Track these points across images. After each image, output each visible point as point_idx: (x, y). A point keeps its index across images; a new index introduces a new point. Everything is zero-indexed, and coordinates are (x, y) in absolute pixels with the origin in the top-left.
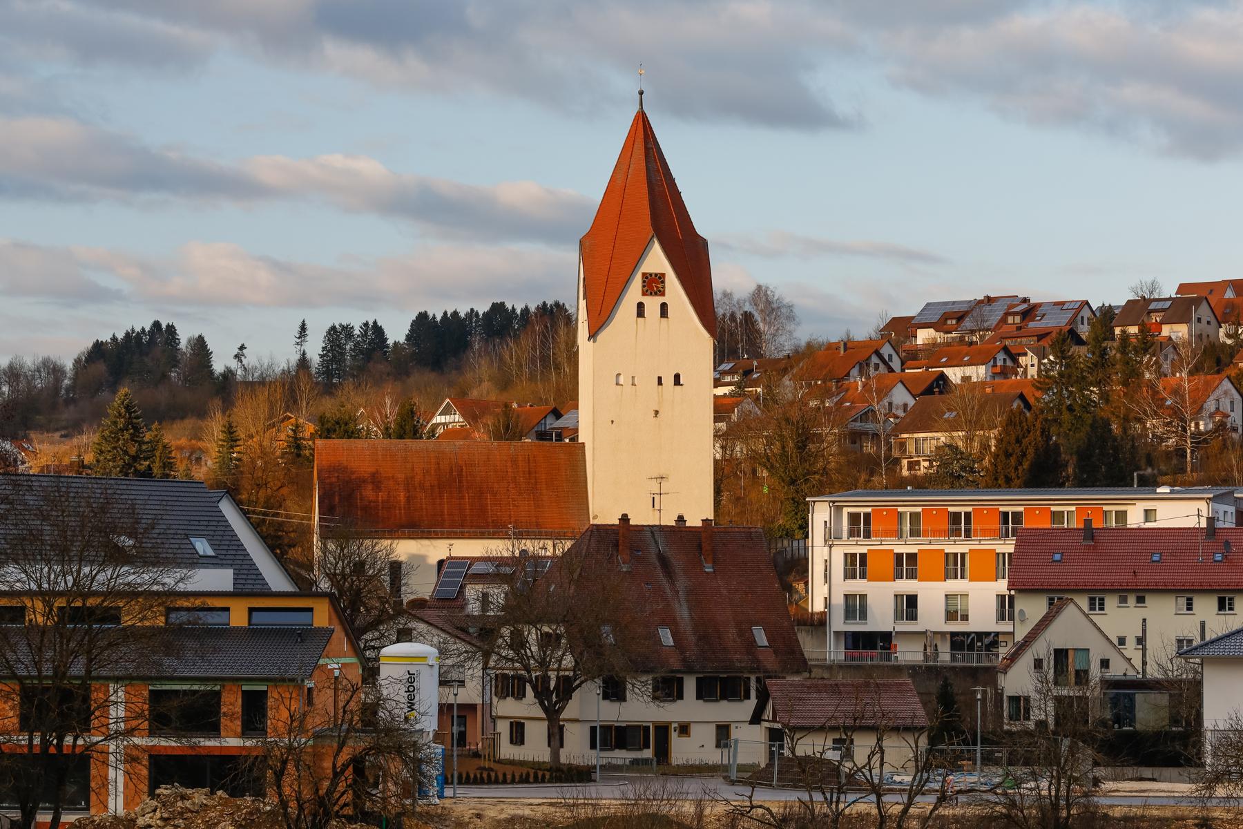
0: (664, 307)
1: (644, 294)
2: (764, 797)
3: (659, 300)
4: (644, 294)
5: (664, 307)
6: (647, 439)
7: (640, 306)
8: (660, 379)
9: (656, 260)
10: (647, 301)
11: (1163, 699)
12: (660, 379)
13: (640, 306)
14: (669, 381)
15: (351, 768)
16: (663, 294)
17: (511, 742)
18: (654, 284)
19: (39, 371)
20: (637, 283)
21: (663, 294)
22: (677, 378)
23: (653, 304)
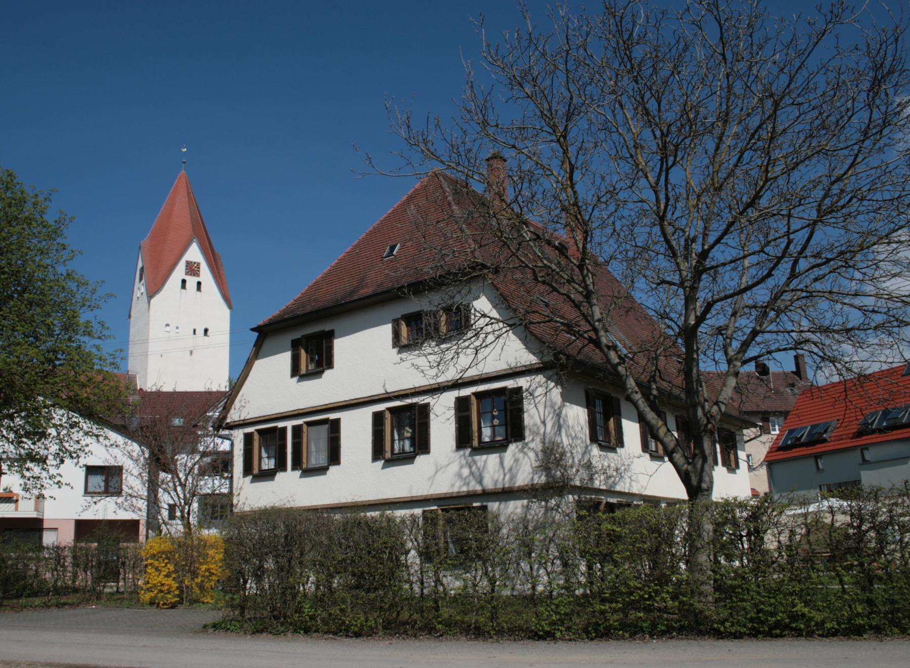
0: (199, 284)
1: (187, 274)
2: (853, 286)
3: (196, 279)
4: (187, 274)
5: (199, 284)
6: (122, 552)
7: (184, 281)
8: (195, 331)
9: (194, 253)
10: (188, 278)
11: (225, 490)
12: (195, 331)
13: (184, 281)
14: (200, 332)
15: (150, 532)
16: (198, 276)
17: (378, 452)
18: (192, 269)
19: (717, 507)
20: (181, 267)
21: (198, 276)
22: (206, 331)
23: (192, 281)
